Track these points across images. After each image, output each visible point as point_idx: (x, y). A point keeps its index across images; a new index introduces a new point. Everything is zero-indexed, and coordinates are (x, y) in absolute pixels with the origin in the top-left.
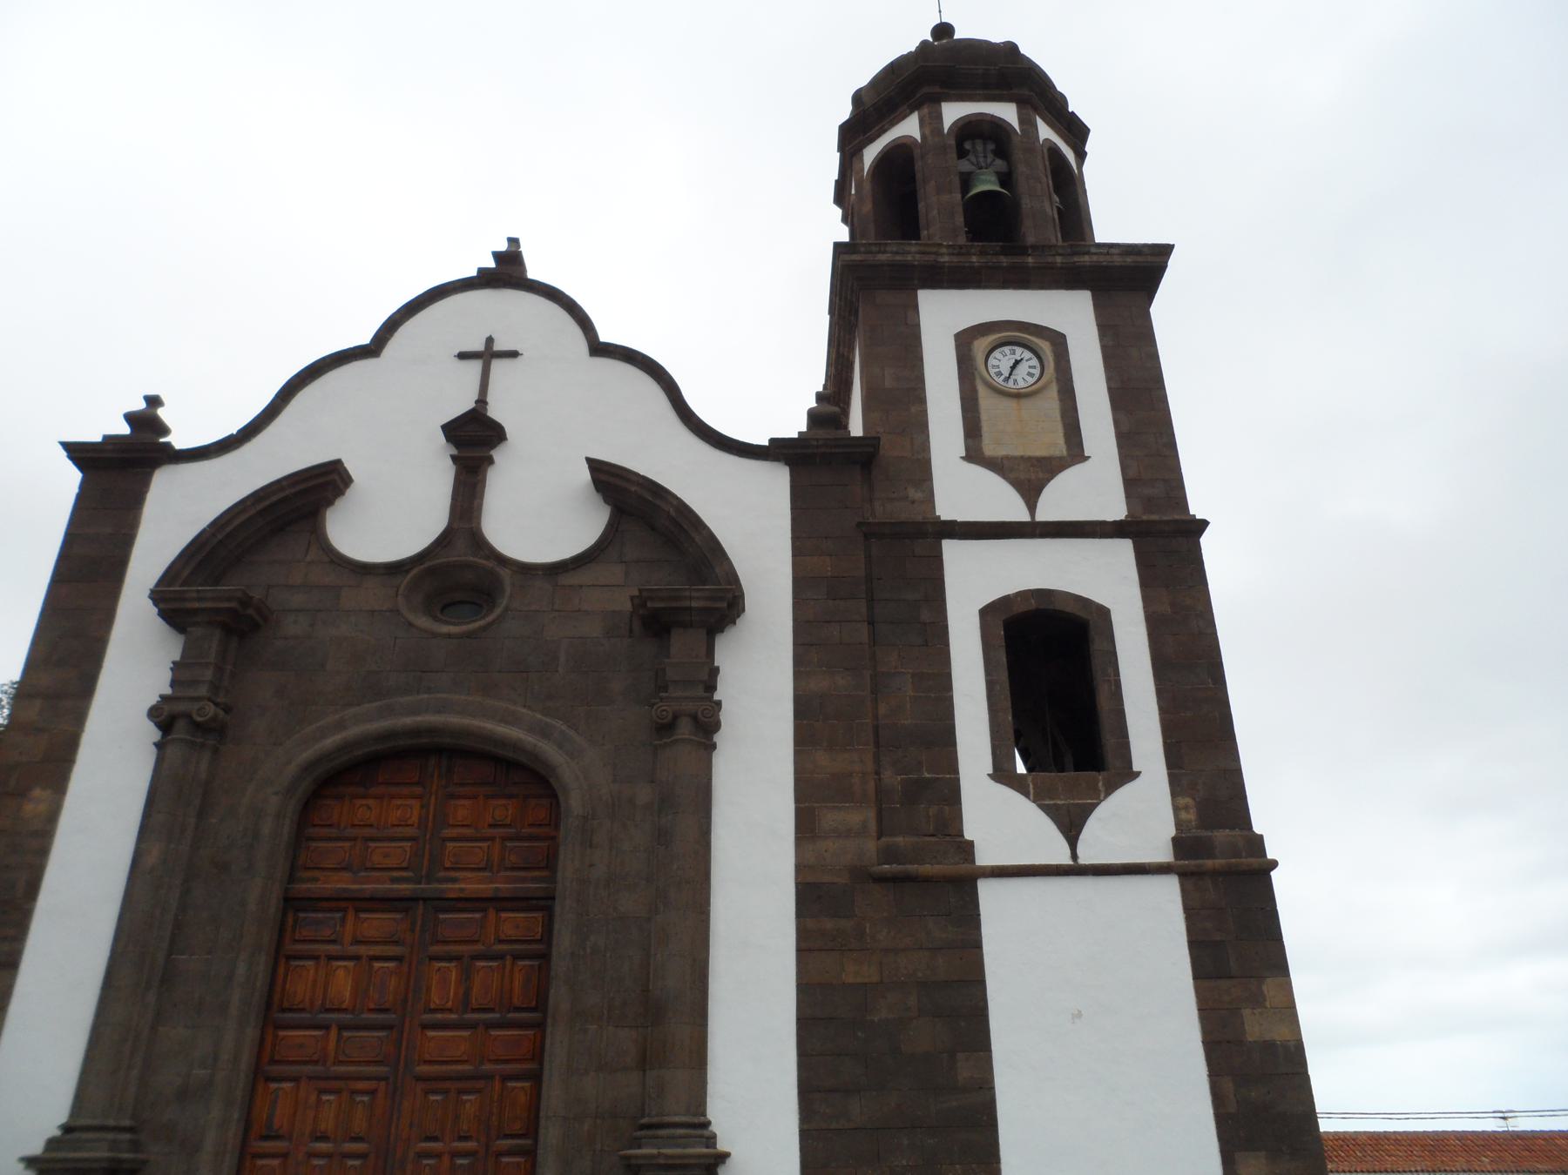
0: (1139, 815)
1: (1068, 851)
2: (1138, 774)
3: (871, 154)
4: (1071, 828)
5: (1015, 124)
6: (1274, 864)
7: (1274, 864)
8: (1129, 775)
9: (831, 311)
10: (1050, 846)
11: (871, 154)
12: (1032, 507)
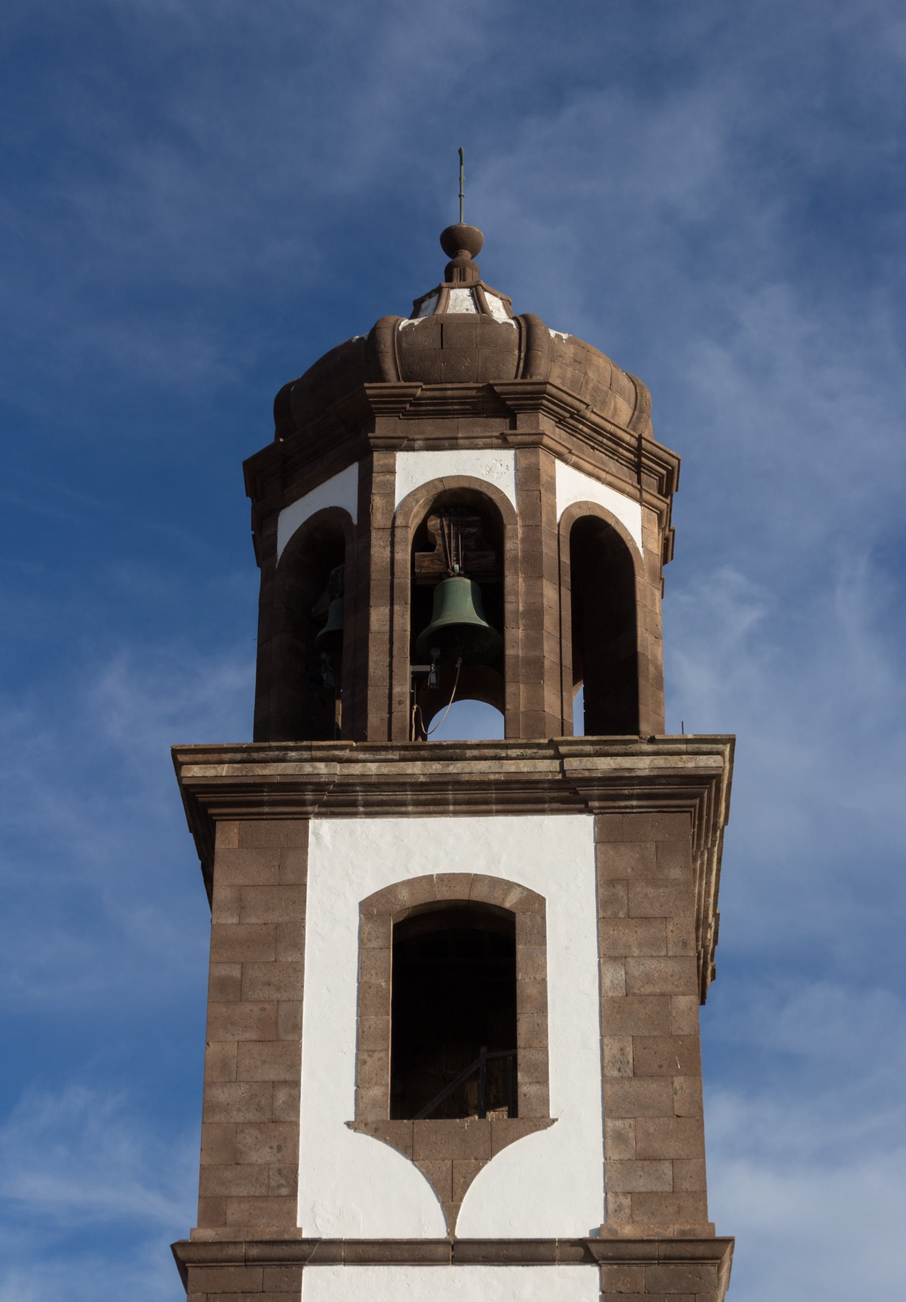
3: (291, 521)
4: (450, 1196)
5: (509, 490)
11: (291, 521)
12: (451, 1212)
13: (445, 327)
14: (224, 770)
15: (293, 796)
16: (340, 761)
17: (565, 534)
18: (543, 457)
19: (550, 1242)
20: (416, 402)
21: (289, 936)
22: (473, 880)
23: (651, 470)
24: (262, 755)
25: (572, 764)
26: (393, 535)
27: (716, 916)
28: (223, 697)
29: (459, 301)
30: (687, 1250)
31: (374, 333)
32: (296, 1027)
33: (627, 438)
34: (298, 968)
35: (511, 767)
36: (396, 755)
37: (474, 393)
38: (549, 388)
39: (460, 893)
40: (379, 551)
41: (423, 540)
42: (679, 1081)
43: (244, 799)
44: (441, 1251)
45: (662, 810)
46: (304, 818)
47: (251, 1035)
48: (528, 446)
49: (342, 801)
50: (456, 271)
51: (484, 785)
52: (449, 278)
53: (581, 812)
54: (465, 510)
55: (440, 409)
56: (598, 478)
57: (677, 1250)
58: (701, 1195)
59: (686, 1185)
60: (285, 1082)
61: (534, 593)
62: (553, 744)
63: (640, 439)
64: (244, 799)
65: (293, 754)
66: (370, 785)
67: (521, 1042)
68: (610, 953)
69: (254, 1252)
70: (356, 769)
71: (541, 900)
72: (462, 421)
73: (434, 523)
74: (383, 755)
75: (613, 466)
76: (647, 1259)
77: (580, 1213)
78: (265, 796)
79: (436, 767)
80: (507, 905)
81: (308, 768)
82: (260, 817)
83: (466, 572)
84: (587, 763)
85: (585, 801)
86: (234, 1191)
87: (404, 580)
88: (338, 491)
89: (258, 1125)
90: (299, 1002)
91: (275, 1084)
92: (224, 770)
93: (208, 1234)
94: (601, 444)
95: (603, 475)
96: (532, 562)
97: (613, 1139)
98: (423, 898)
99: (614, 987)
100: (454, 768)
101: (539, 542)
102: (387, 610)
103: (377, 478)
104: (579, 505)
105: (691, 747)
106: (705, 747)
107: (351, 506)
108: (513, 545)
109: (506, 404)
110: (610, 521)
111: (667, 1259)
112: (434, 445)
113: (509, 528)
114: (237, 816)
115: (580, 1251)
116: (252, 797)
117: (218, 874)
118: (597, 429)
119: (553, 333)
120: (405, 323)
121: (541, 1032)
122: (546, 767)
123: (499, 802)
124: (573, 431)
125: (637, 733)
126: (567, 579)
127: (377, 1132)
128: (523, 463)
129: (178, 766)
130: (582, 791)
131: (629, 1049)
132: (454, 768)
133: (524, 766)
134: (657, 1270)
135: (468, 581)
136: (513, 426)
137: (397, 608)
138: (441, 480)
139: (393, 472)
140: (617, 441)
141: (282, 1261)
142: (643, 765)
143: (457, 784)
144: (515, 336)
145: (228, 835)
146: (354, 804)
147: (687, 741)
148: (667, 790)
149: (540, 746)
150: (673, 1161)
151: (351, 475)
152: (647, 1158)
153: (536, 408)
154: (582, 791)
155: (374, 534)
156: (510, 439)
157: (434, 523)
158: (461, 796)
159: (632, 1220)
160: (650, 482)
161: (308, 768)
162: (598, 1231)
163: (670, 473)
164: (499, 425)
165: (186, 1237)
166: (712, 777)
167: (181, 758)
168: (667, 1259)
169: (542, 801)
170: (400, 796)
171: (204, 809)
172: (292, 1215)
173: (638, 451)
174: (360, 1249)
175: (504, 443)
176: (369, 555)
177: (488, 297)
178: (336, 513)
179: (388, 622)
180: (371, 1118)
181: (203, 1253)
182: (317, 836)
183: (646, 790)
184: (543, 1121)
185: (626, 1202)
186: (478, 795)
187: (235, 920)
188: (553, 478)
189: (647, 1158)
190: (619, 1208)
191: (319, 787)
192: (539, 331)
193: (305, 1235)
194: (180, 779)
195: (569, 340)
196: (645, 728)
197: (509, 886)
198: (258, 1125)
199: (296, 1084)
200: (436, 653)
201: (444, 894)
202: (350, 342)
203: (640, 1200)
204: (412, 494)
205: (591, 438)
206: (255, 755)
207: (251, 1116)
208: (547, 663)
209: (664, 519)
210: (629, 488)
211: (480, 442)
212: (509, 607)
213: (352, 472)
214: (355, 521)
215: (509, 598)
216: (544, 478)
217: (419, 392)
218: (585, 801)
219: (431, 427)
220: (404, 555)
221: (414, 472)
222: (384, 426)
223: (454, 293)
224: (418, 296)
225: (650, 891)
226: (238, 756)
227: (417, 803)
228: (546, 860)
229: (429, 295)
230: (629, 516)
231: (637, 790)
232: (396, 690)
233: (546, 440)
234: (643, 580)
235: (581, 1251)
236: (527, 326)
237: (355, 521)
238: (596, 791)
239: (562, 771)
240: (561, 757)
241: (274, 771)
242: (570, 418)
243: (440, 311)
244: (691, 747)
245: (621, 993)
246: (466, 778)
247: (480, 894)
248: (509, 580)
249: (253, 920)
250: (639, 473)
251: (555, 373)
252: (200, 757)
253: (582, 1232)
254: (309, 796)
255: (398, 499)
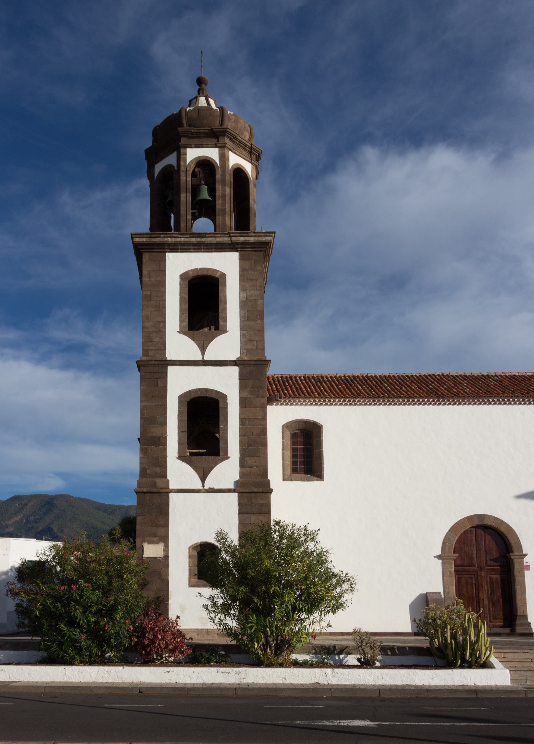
0: (227, 471)
1: (201, 485)
2: (229, 457)
3: (158, 168)
4: (203, 349)
5: (217, 161)
6: (439, 557)
7: (439, 557)
8: (227, 457)
9: (164, 741)
10: (194, 481)
11: (158, 168)
12: (203, 353)
13: (200, 110)
14: (144, 240)
15: (162, 247)
16: (174, 237)
17: (232, 173)
18: (226, 150)
19: (227, 361)
20: (192, 133)
21: (162, 284)
22: (208, 269)
23: (254, 154)
24: (154, 236)
25: (234, 239)
26: (186, 173)
27: (267, 277)
28: (138, 216)
29: (202, 102)
30: (260, 363)
31: (180, 112)
32: (164, 307)
33: (248, 144)
34: (164, 292)
35: (218, 239)
36: (188, 236)
37: (208, 131)
38: (228, 130)
39: (205, 273)
40: (183, 178)
41: (194, 175)
42: (259, 321)
43: (150, 247)
44: (201, 363)
45: (256, 251)
46: (165, 252)
47: (154, 309)
48: (222, 147)
49: (176, 248)
50: (201, 91)
51: (211, 244)
52: (199, 93)
53: (235, 251)
54: (205, 164)
55: (198, 135)
56: (240, 156)
57: (257, 363)
58: (263, 350)
59: (260, 347)
60: (162, 321)
61: (224, 190)
62: (229, 233)
63: (252, 144)
64: (150, 247)
65: (162, 235)
66: (182, 244)
67: (220, 311)
68: (242, 289)
69: (156, 363)
70: (178, 240)
71: (225, 275)
72: (204, 139)
73: (197, 169)
74: (185, 236)
75: (244, 153)
76: (250, 365)
77: (234, 354)
78: (155, 247)
79: (199, 239)
80: (217, 276)
81: (166, 239)
82: (154, 252)
83: (206, 184)
84: (238, 238)
85: (237, 249)
86: (151, 348)
87: (189, 186)
88: (171, 160)
89: (156, 332)
90: (164, 301)
91: (160, 322)
92: (144, 240)
93: (145, 359)
94: (241, 146)
95: (242, 155)
96: (223, 181)
97: (242, 336)
98: (196, 274)
99: (243, 298)
100: (204, 239)
101: (225, 175)
102: (185, 195)
103: (182, 156)
104: (235, 164)
105: (264, 234)
106: (268, 234)
107: (175, 164)
108: (218, 177)
109: (215, 133)
110: (243, 169)
111: (255, 365)
112: (197, 146)
113: (217, 171)
114: (148, 252)
115: (234, 363)
116: (151, 247)
117: (144, 267)
118: (240, 142)
119: (229, 112)
120: (188, 109)
121: (225, 309)
122: (227, 239)
123: (215, 249)
124: (234, 142)
125: (249, 230)
126: (232, 186)
127: (185, 334)
128: (221, 152)
129: (132, 238)
130: (236, 246)
131: (247, 313)
132: (204, 239)
133: (221, 239)
134: (252, 367)
135: (206, 187)
136: (218, 141)
137: (188, 194)
138: (199, 157)
139: (186, 154)
140: (245, 145)
141: (163, 365)
142: (252, 239)
143: (204, 244)
144: (219, 114)
145: (146, 257)
146: (178, 249)
147: (263, 233)
148: (258, 246)
149: (225, 234)
150: (257, 341)
151: (174, 155)
152: (250, 340)
153: (224, 136)
154: (236, 246)
155: (181, 173)
156: (218, 145)
157: (197, 169)
158: (205, 247)
159: (246, 355)
160: (254, 157)
161: (166, 239)
162: (238, 358)
163: (259, 155)
164: (214, 141)
165: (140, 359)
166: (269, 243)
167: (133, 236)
168: (255, 365)
169: (225, 248)
170: (189, 247)
171: (139, 250)
172: (165, 354)
173: (251, 148)
174: (181, 362)
175: (216, 146)
176: (180, 179)
177: (210, 99)
178: (170, 166)
179: (185, 198)
180: (183, 330)
181: (144, 363)
182: (169, 258)
183: (252, 246)
184: (225, 331)
185: (245, 351)
186: (209, 247)
187: (148, 280)
188: (229, 157)
189: (250, 340)
190: (243, 353)
191: (169, 244)
192: (225, 112)
193: (168, 359)
194: (133, 242)
195: (233, 114)
196: (251, 228)
197: (217, 271)
198: (156, 332)
199: (165, 322)
200: (197, 207)
201: (201, 273)
202: (173, 114)
203: (249, 351)
204: (191, 161)
205: (239, 144)
206: (152, 236)
207: (154, 330)
208: (227, 210)
209: (257, 168)
210: (248, 159)
211: (210, 146)
212: (217, 194)
213: (175, 154)
214: (176, 169)
215: (217, 192)
216: (226, 156)
217: (193, 131)
218: (237, 249)
219: (196, 141)
220: (189, 179)
221: (192, 154)
222: (183, 141)
223: (201, 98)
224: (190, 99)
225: (253, 273)
226: (148, 236)
227: (194, 249)
228: (227, 264)
229: (194, 99)
230: (248, 167)
231: (250, 246)
232: (188, 217)
233: (227, 145)
234: (251, 186)
235: (234, 363)
236: (222, 109)
237: (176, 169)
238: (240, 246)
239: (231, 240)
240: (231, 237)
241: (157, 240)
242: (233, 138)
243: (197, 105)
244: (264, 234)
245: (245, 299)
246: (206, 242)
247: (210, 273)
248: (217, 186)
249: (153, 280)
250: (251, 155)
251: (229, 125)
252: (138, 236)
253: (234, 358)
254: (166, 247)
255: (187, 163)
